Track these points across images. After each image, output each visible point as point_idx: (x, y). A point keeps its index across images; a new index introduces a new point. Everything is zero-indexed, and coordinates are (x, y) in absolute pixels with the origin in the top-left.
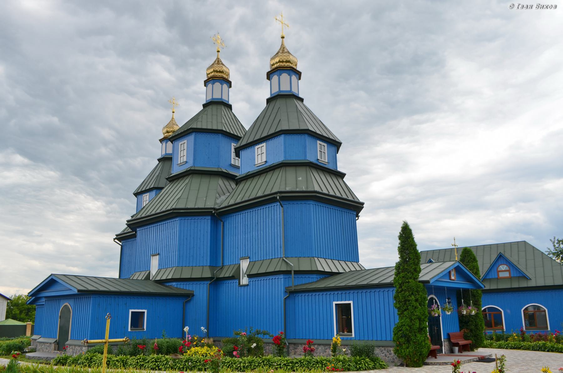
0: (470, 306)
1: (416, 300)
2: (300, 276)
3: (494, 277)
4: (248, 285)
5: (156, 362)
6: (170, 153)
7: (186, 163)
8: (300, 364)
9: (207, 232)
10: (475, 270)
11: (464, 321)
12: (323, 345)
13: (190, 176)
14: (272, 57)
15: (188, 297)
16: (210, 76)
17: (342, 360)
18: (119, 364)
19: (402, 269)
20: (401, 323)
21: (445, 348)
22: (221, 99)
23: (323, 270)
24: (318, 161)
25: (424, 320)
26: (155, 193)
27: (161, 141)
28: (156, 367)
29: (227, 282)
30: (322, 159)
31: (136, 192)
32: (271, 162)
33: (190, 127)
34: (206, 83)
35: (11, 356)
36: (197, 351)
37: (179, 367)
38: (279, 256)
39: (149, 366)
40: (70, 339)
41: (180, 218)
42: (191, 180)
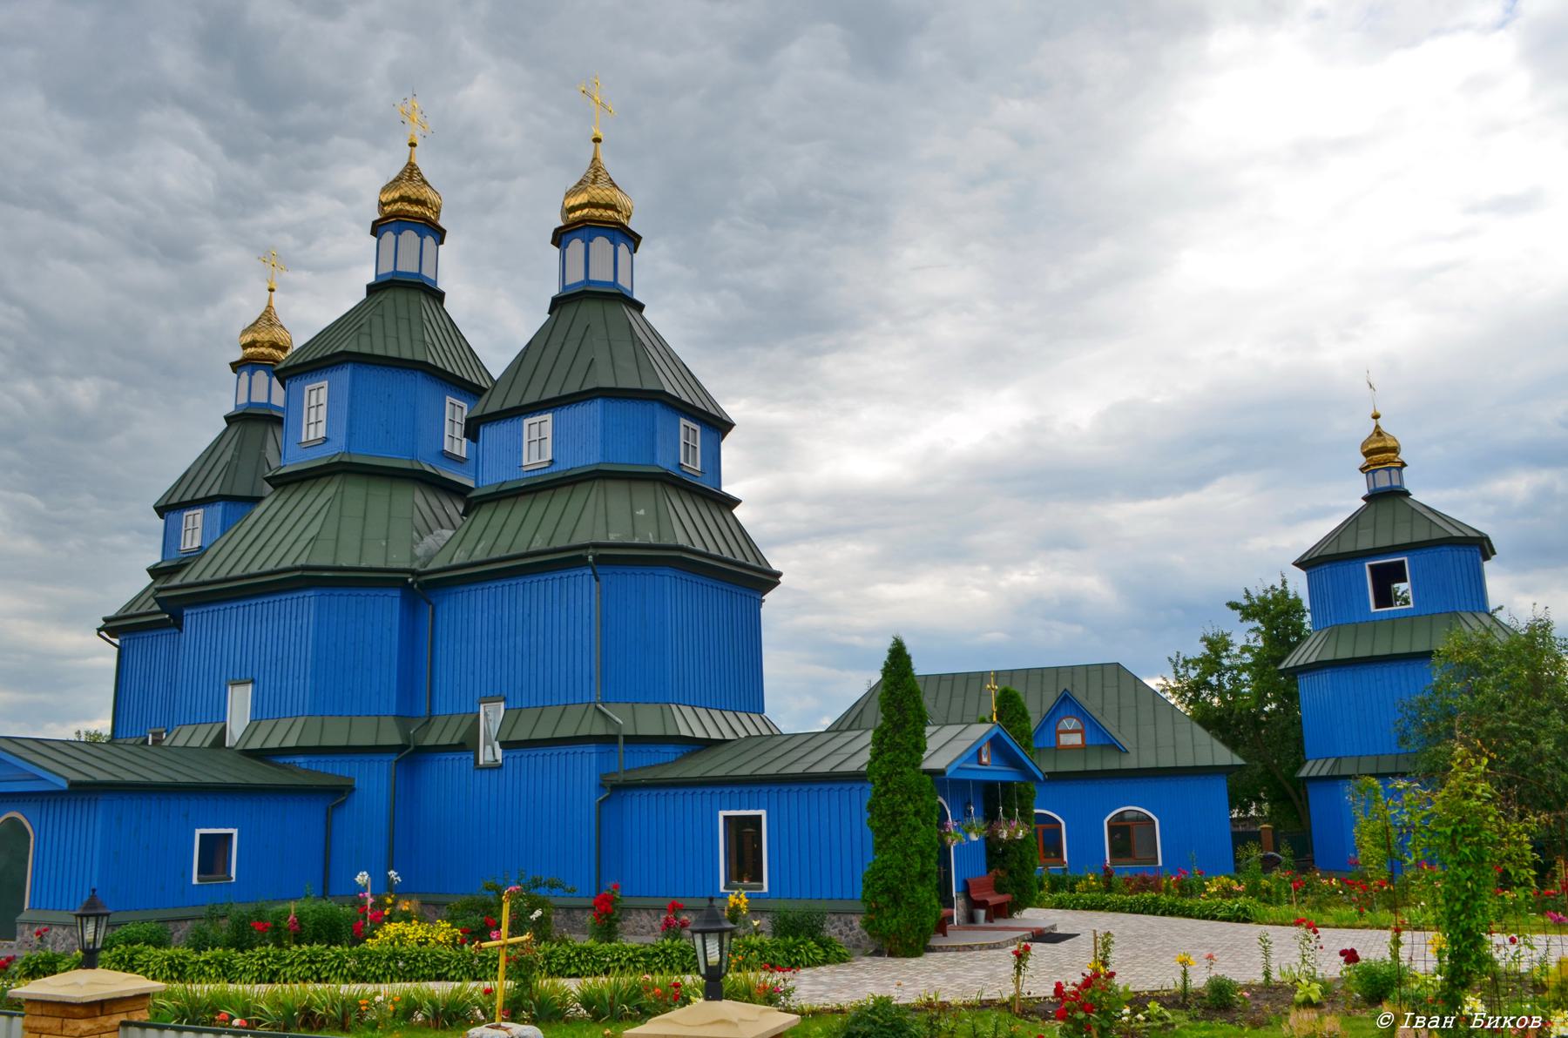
0: (1014, 820)
1: (917, 813)
2: (636, 748)
3: (1048, 746)
4: (500, 767)
5: (312, 962)
7: (325, 442)
8: (664, 957)
9: (390, 630)
10: (1025, 739)
11: (995, 852)
12: (692, 910)
13: (338, 479)
14: (568, 190)
15: (339, 793)
16: (390, 209)
17: (757, 946)
18: (212, 971)
19: (887, 745)
20: (883, 861)
21: (957, 913)
22: (419, 274)
23: (690, 734)
24: (680, 469)
25: (930, 856)
26: (220, 513)
27: (236, 367)
28: (311, 976)
29: (443, 756)
30: (688, 463)
31: (163, 503)
32: (567, 465)
33: (341, 349)
34: (377, 229)
35: (1552, 985)
36: (401, 932)
37: (374, 973)
38: (586, 699)
39: (296, 972)
40: (29, 909)
42: (340, 490)
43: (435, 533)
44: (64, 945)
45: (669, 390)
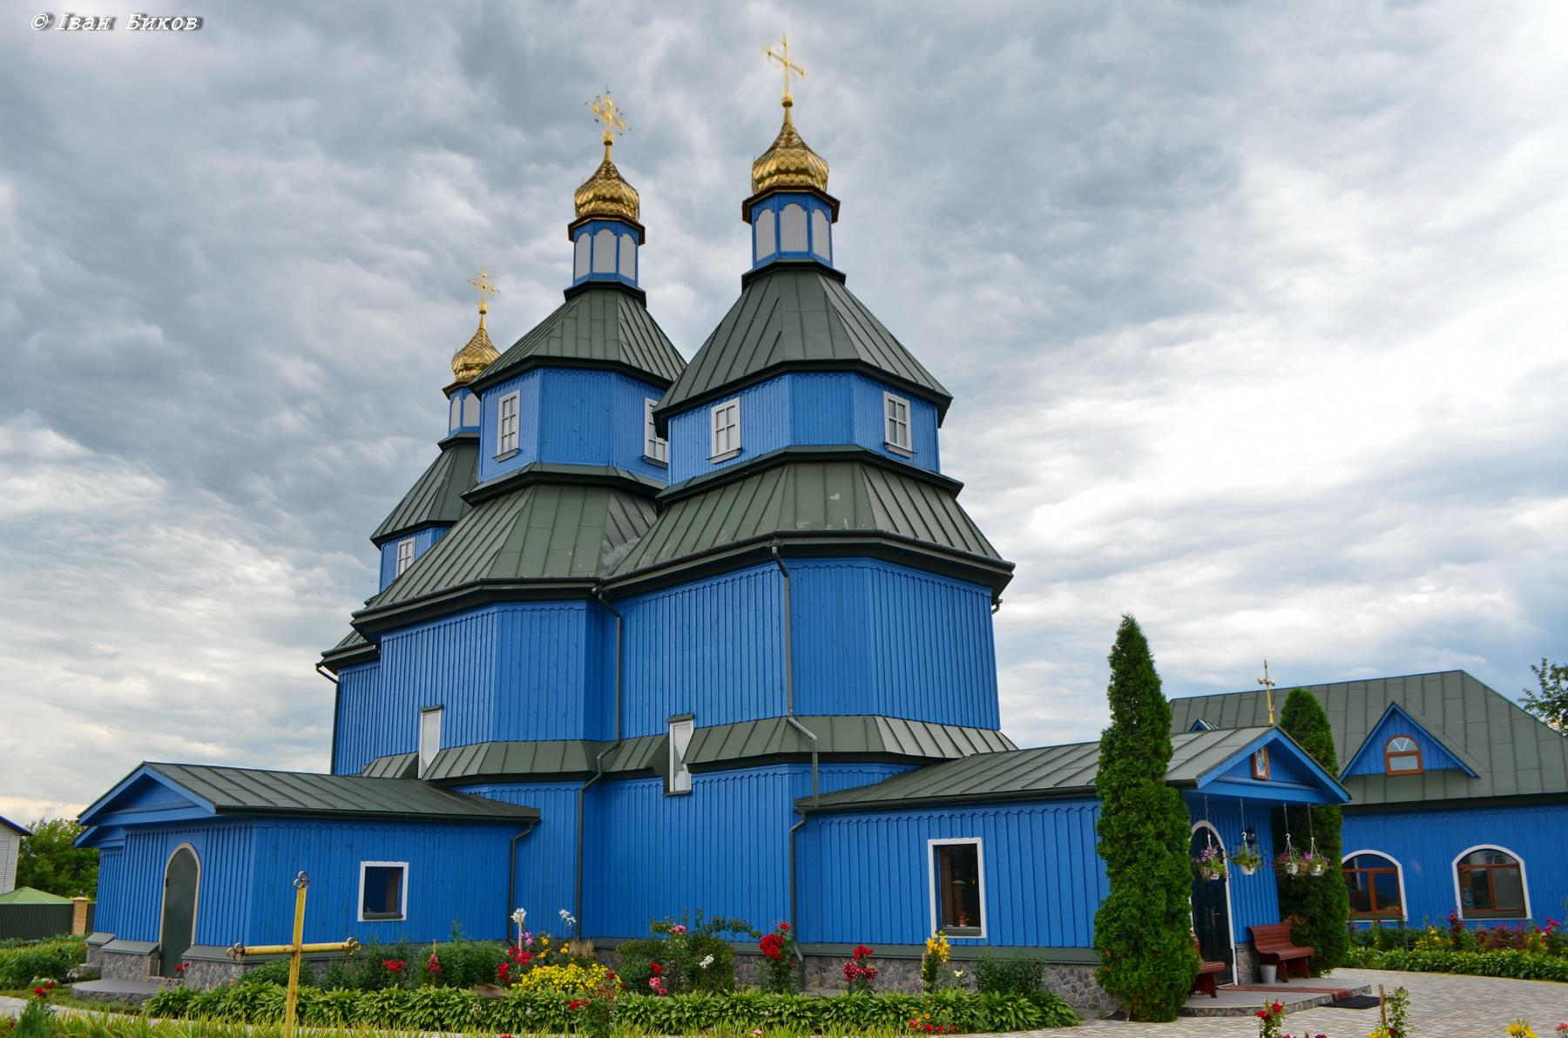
0: (1309, 853)
1: (1160, 836)
2: (835, 768)
3: (1376, 772)
4: (689, 794)
5: (435, 1006)
6: (473, 425)
7: (518, 454)
8: (837, 1012)
9: (576, 646)
10: (1324, 751)
11: (1292, 894)
12: (899, 959)
13: (530, 490)
15: (523, 825)
16: (585, 210)
18: (331, 1013)
19: (1119, 749)
20: (1117, 898)
21: (1239, 969)
23: (898, 751)
24: (886, 449)
27: (449, 391)
28: (433, 1022)
29: (633, 784)
30: (896, 442)
32: (754, 453)
34: (574, 231)
37: (500, 1021)
38: (778, 713)
39: (416, 1018)
40: (195, 944)
41: (502, 608)
42: (531, 501)
43: (629, 542)
44: (219, 984)
45: (866, 358)
